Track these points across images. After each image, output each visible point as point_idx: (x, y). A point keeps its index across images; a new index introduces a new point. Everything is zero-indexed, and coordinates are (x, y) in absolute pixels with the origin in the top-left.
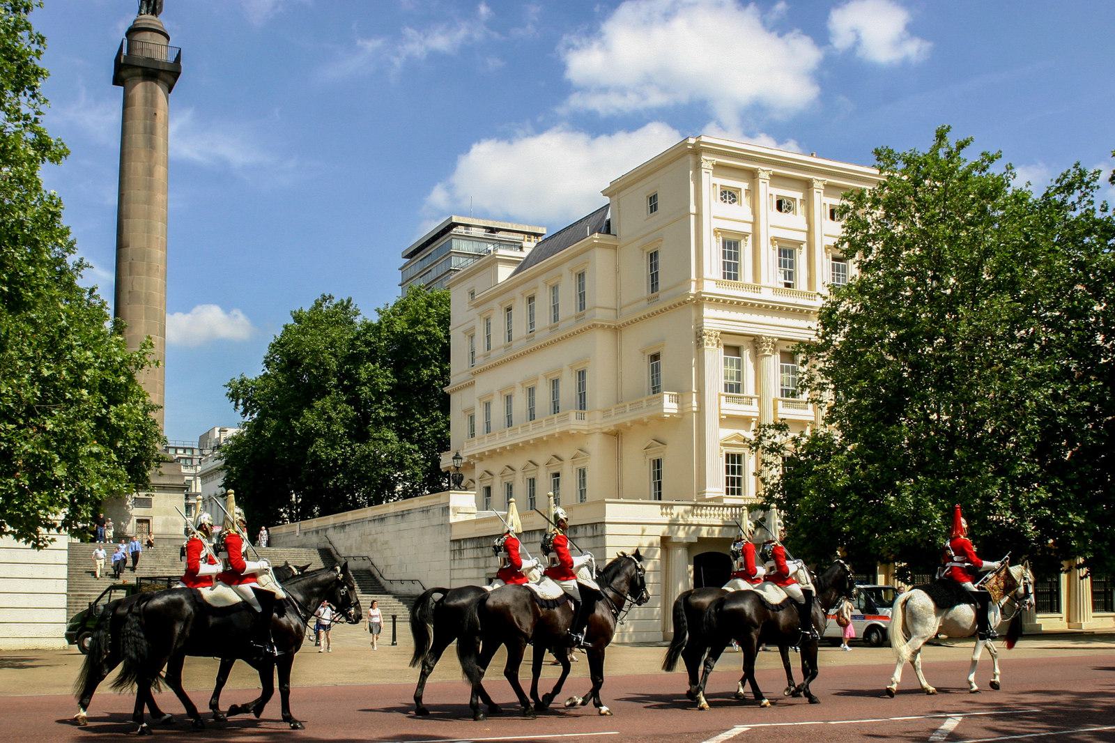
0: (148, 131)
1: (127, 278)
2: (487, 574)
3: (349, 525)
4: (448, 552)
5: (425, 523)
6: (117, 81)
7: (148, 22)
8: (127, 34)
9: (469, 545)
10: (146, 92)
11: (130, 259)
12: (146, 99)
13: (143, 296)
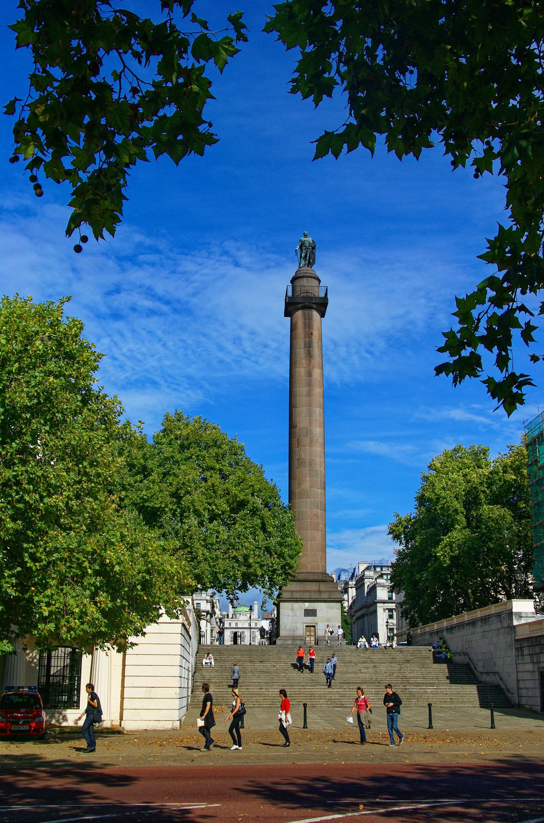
0: (307, 345)
1: (296, 449)
2: (538, 668)
3: (455, 627)
4: (514, 650)
5: (499, 625)
6: (287, 313)
7: (305, 271)
8: (292, 281)
9: (525, 644)
10: (305, 319)
11: (297, 437)
12: (305, 325)
13: (307, 461)
